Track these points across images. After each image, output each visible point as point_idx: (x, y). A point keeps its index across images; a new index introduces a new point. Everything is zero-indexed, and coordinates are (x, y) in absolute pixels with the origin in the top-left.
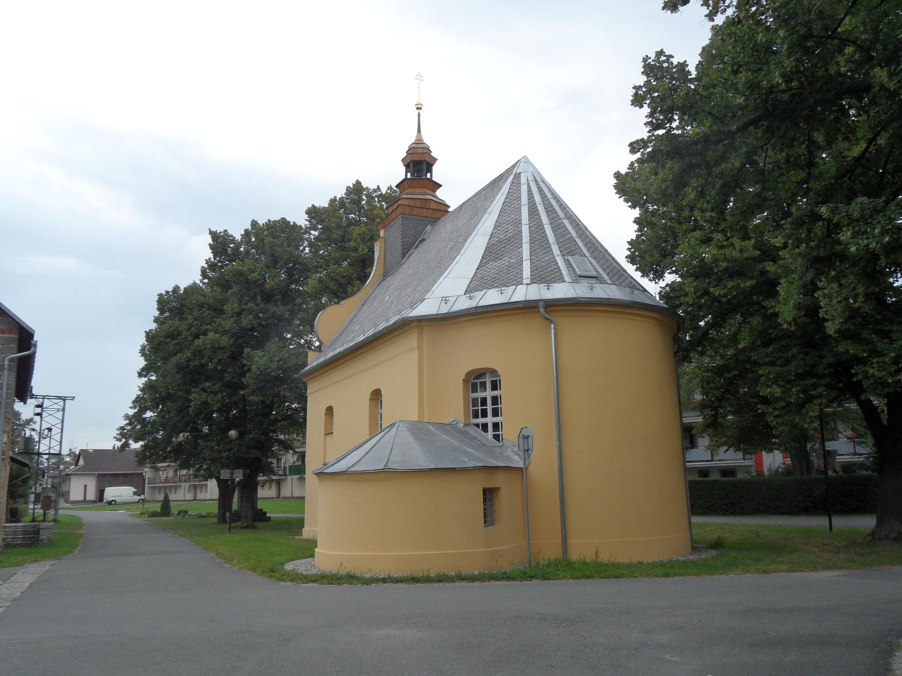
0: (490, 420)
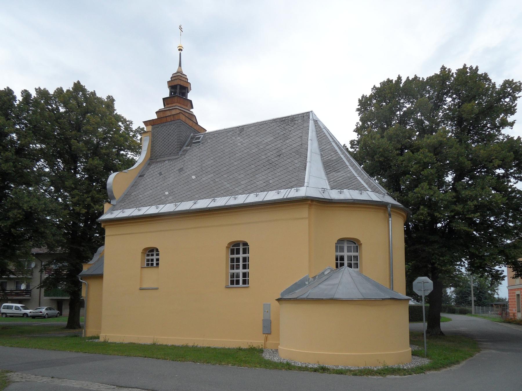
0: (241, 256)
